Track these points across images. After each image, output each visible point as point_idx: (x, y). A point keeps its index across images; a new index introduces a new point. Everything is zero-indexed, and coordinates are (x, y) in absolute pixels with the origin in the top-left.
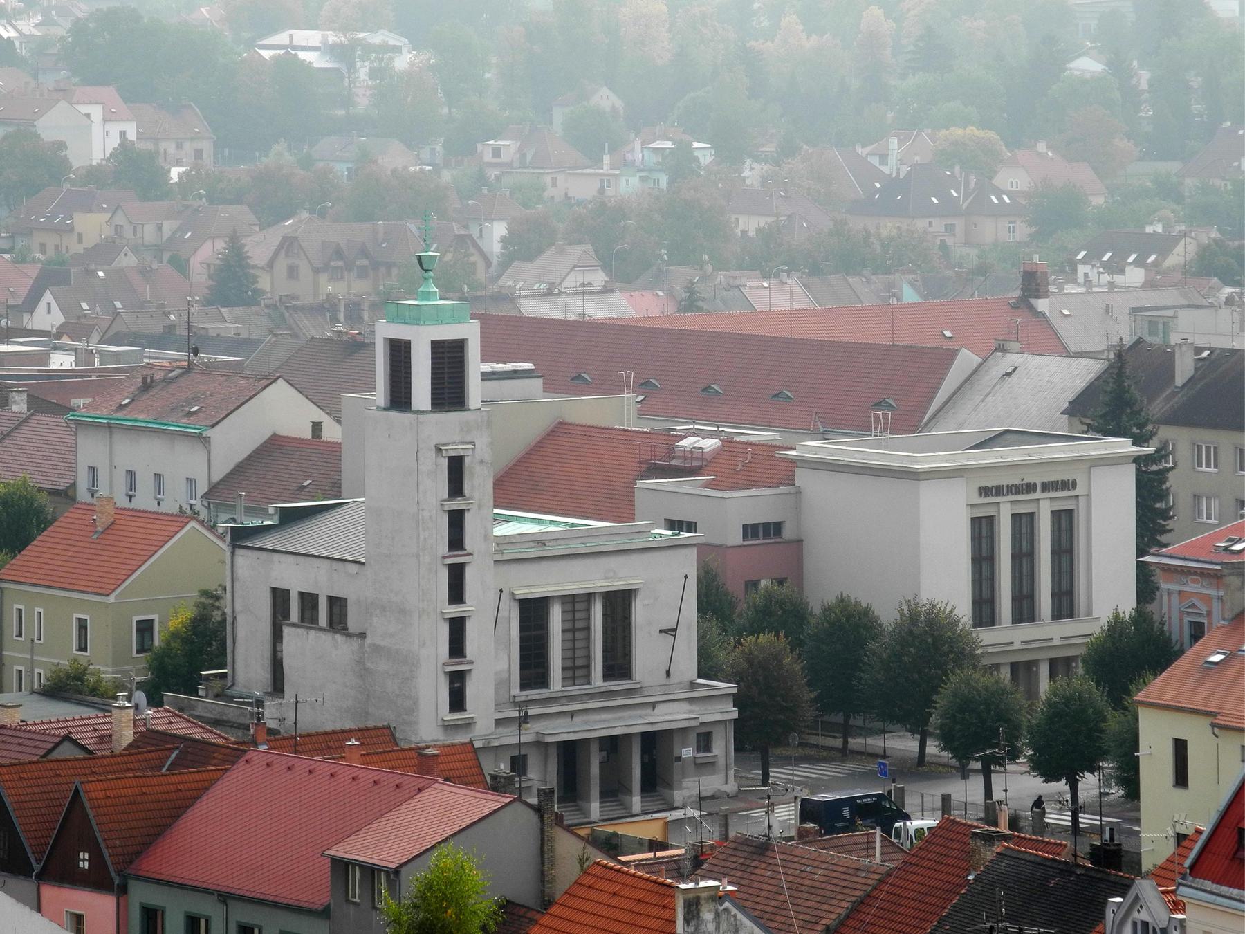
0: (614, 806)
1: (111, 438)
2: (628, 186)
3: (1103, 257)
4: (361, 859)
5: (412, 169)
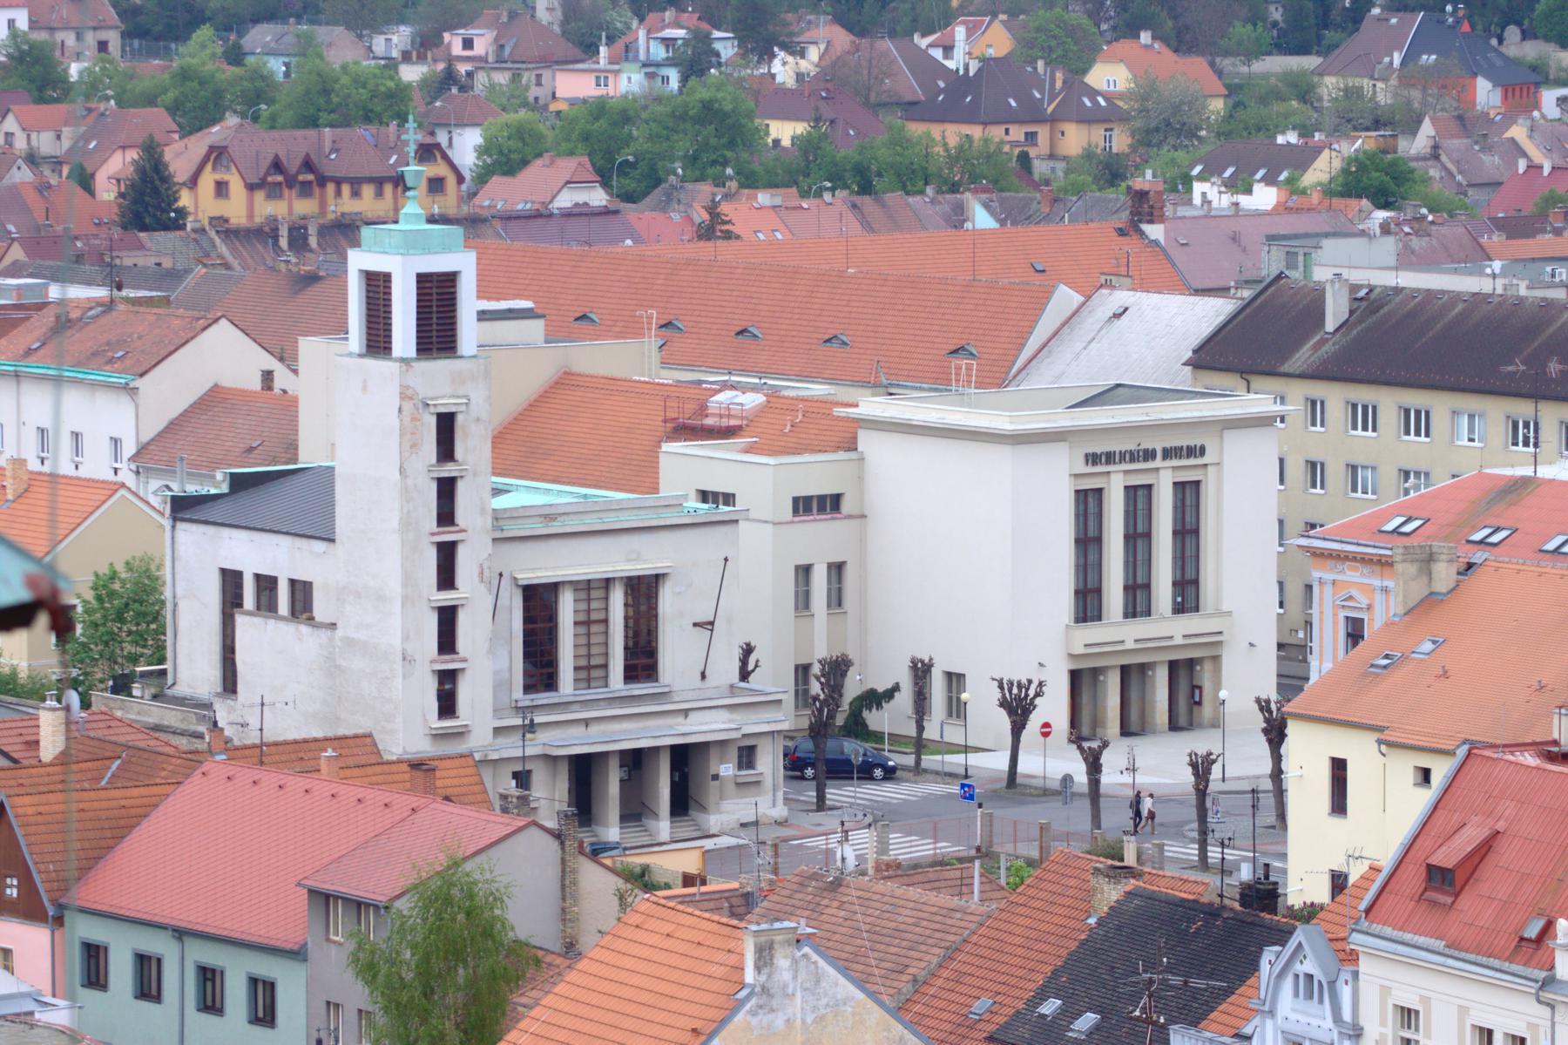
1: (18, 393)
2: (629, 82)
4: (344, 890)
5: (365, 63)
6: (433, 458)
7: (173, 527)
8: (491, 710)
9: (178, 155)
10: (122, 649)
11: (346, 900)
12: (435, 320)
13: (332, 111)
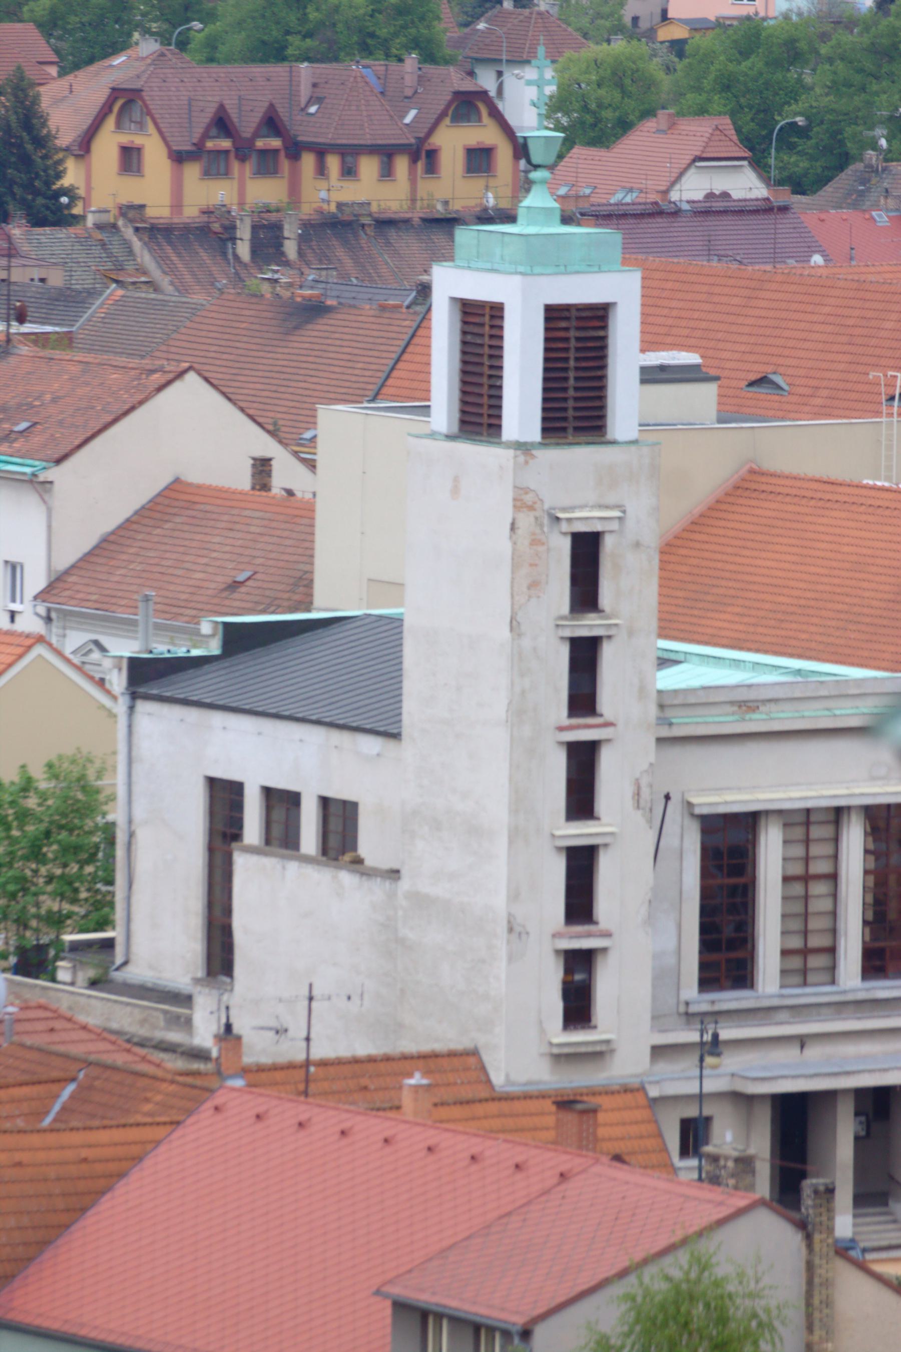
0: (879, 1223)
3: (404, 117)
6: (565, 606)
7: (132, 708)
8: (647, 1017)
9: (58, 101)
10: (38, 905)
11: (457, 1321)
12: (572, 382)
13: (309, 35)
